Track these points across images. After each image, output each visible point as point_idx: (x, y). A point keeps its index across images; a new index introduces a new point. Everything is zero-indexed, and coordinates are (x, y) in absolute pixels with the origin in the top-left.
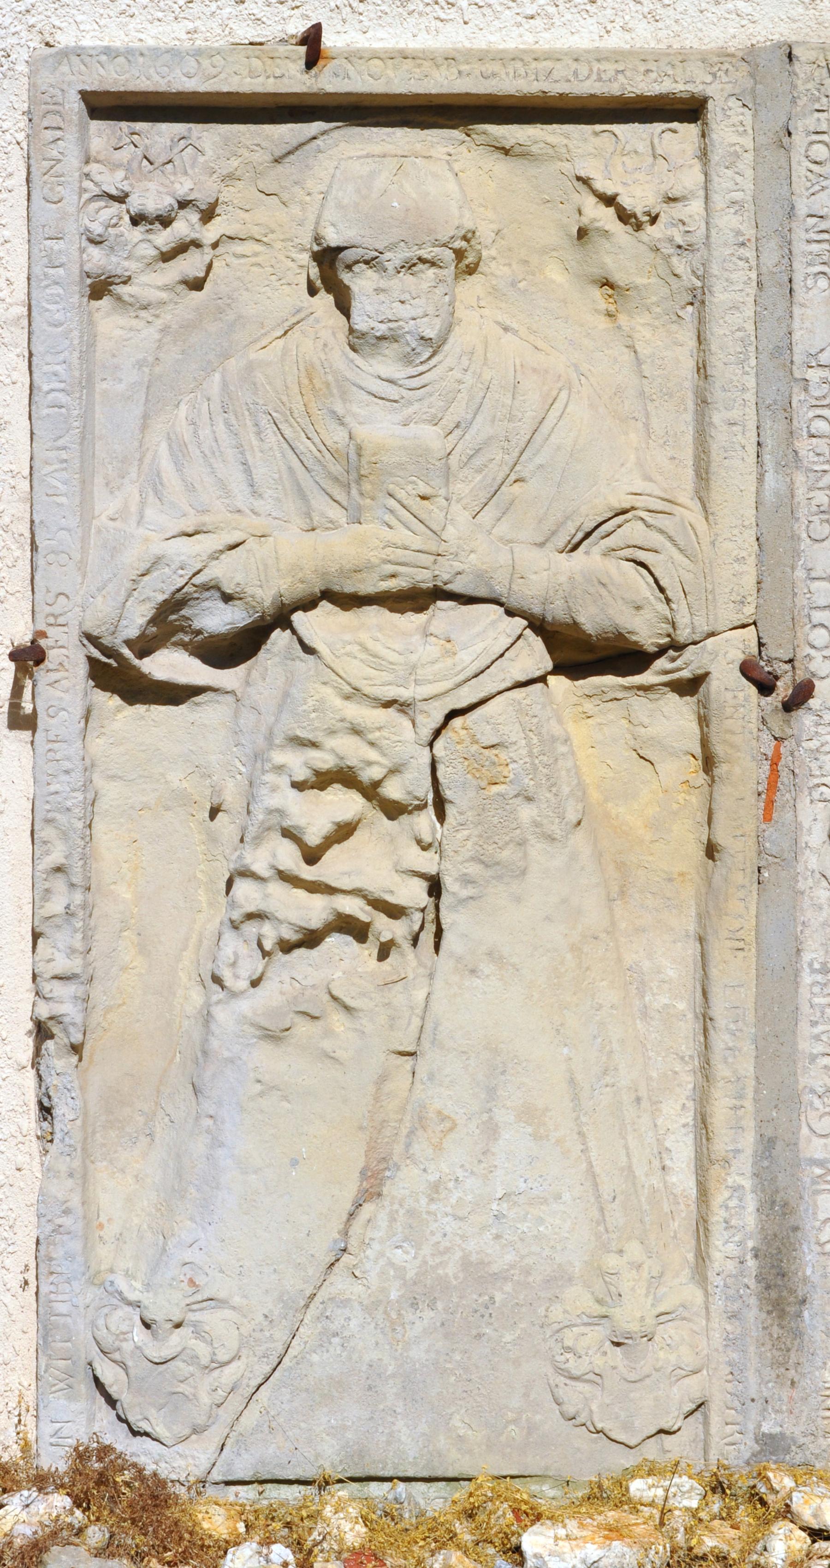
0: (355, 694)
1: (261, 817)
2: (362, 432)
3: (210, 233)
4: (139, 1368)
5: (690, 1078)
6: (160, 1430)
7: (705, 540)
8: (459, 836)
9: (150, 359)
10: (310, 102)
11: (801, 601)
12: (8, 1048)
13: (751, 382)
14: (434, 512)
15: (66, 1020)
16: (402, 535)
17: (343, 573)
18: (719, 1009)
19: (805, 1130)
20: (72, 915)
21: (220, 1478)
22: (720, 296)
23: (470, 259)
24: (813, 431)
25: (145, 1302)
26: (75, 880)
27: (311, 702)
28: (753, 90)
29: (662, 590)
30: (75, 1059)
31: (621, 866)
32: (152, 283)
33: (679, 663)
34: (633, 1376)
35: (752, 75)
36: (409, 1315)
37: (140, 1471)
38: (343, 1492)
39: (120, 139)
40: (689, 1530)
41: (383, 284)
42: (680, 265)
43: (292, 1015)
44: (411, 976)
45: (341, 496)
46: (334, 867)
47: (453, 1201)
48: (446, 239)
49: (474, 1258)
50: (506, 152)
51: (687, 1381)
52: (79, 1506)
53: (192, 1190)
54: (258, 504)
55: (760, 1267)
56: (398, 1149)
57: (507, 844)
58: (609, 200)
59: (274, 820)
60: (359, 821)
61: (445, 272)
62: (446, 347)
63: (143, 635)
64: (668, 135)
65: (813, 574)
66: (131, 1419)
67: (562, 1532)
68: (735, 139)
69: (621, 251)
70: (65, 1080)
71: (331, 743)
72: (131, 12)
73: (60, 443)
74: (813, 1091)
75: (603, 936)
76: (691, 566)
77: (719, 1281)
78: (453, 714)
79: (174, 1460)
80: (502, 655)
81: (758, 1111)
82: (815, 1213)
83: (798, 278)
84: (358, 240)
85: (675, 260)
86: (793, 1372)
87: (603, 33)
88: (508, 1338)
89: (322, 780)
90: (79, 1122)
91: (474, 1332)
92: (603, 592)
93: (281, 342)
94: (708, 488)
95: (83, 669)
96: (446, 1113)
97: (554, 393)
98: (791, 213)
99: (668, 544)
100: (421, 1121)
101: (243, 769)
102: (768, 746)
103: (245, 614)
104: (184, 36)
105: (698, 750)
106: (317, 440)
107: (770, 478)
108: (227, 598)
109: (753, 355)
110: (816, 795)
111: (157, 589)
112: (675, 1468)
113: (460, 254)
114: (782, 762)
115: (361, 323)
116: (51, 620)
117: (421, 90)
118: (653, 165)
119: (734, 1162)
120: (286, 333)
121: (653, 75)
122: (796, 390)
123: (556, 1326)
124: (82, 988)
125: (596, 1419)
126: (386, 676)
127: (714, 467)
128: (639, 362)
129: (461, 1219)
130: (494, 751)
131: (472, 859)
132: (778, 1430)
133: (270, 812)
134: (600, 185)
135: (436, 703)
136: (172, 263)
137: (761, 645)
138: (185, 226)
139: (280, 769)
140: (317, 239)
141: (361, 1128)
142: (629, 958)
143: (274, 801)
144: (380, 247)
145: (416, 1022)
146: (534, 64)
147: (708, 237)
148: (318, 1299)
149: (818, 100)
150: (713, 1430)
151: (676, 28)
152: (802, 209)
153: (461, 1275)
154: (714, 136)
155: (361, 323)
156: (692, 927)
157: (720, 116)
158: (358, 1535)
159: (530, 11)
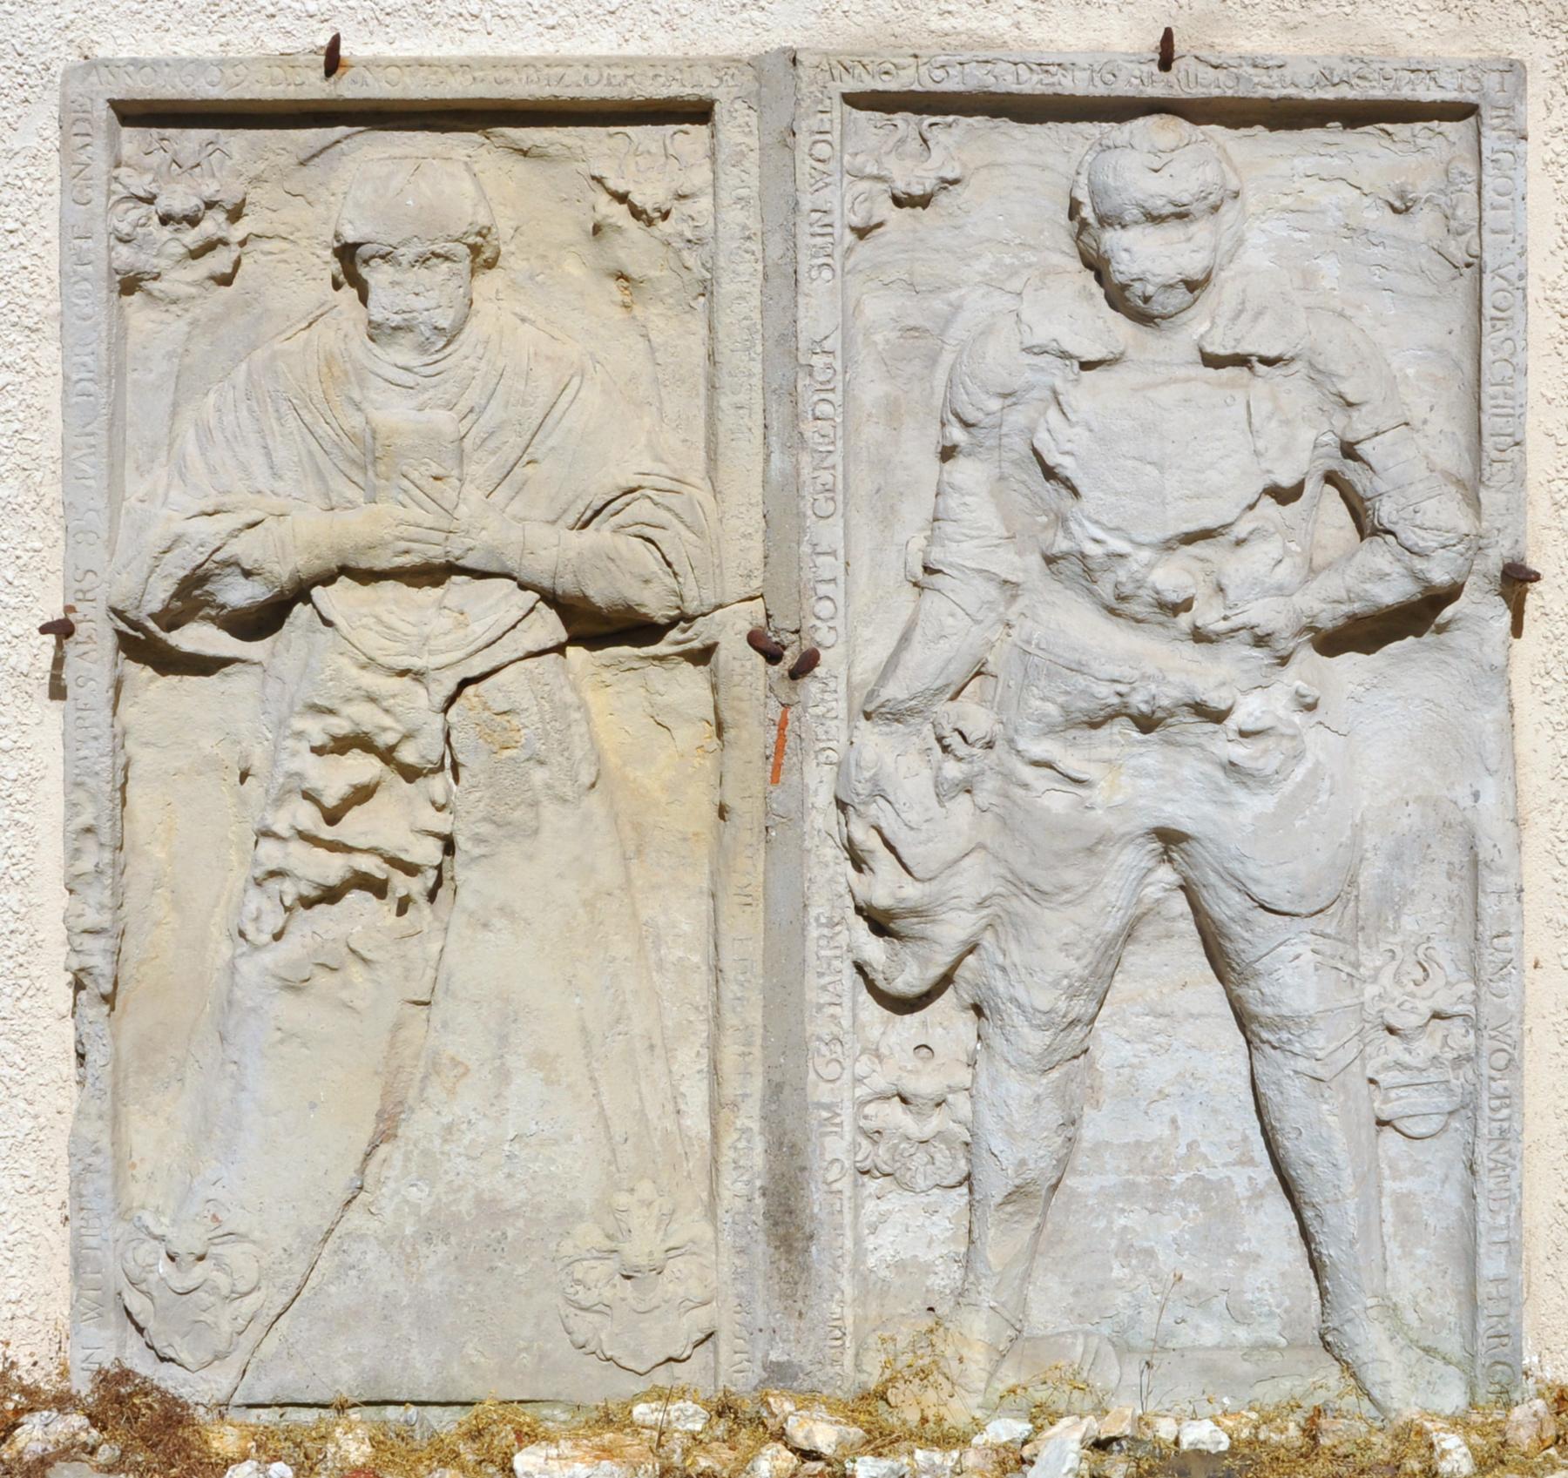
0: (369, 664)
1: (281, 780)
2: (378, 417)
3: (238, 232)
5: (704, 1027)
6: (184, 1356)
8: (471, 797)
9: (180, 350)
10: (334, 108)
11: (807, 574)
12: (49, 999)
13: (757, 368)
14: (447, 491)
15: (96, 971)
16: (415, 514)
17: (358, 549)
19: (812, 1076)
20: (101, 873)
21: (240, 1401)
22: (727, 288)
23: (488, 253)
24: (818, 414)
25: (169, 1236)
26: (103, 840)
27: (328, 672)
28: (758, 93)
29: (669, 565)
30: (106, 1009)
31: (637, 827)
32: (181, 279)
33: (689, 634)
34: (642, 1308)
35: (757, 79)
36: (423, 1249)
37: (164, 1394)
38: (354, 1415)
39: (150, 144)
40: (686, 1452)
41: (398, 277)
42: (690, 259)
43: (311, 967)
44: (426, 930)
45: (358, 478)
46: (352, 828)
47: (466, 1142)
48: (458, 235)
49: (486, 1196)
50: (525, 153)
51: (695, 1312)
52: (94, 1426)
53: (218, 1132)
54: (279, 486)
55: (768, 1205)
56: (413, 1093)
57: (518, 805)
58: (622, 198)
59: (295, 783)
60: (377, 784)
61: (459, 266)
62: (462, 337)
63: (166, 610)
64: (679, 136)
65: (819, 549)
66: (157, 1346)
67: (553, 1452)
68: (740, 139)
69: (636, 247)
70: (97, 1028)
71: (348, 710)
72: (166, 26)
73: (89, 429)
74: (819, 1039)
75: (617, 892)
76: (699, 542)
77: (727, 1218)
78: (465, 683)
79: (195, 1386)
80: (514, 627)
81: (766, 1057)
82: (822, 1154)
84: (372, 236)
85: (685, 253)
86: (800, 1304)
87: (621, 41)
88: (520, 1270)
89: (341, 745)
90: (109, 1068)
91: (487, 1265)
92: (611, 565)
93: (305, 333)
94: (716, 469)
95: (110, 641)
96: (459, 1058)
97: (566, 380)
98: (796, 207)
99: (675, 521)
100: (435, 1067)
101: (270, 736)
102: (775, 712)
103: (264, 589)
104: (217, 49)
105: (712, 717)
106: (335, 425)
107: (776, 458)
108: (247, 574)
109: (759, 342)
110: (822, 758)
111: (178, 566)
112: (683, 1394)
113: (475, 250)
114: (789, 727)
116: (80, 596)
117: (436, 96)
118: (665, 165)
119: (742, 1106)
120: (310, 325)
121: (662, 80)
122: (801, 375)
123: (567, 1260)
124: (112, 942)
125: (605, 1348)
126: (401, 647)
127: (721, 449)
129: (474, 1159)
130: (506, 718)
131: (484, 819)
132: (785, 1358)
133: (290, 775)
134: (612, 184)
135: (448, 672)
136: (201, 260)
137: (768, 616)
138: (212, 225)
139: (299, 735)
140: (337, 236)
141: (376, 1073)
142: (644, 915)
143: (294, 765)
144: (394, 242)
145: (430, 973)
146: (546, 70)
147: (716, 232)
148: (336, 1233)
149: (821, 101)
150: (722, 1359)
151: (693, 36)
153: (474, 1212)
154: (721, 136)
156: (705, 885)
157: (726, 118)
158: (363, 1455)
159: (551, 22)
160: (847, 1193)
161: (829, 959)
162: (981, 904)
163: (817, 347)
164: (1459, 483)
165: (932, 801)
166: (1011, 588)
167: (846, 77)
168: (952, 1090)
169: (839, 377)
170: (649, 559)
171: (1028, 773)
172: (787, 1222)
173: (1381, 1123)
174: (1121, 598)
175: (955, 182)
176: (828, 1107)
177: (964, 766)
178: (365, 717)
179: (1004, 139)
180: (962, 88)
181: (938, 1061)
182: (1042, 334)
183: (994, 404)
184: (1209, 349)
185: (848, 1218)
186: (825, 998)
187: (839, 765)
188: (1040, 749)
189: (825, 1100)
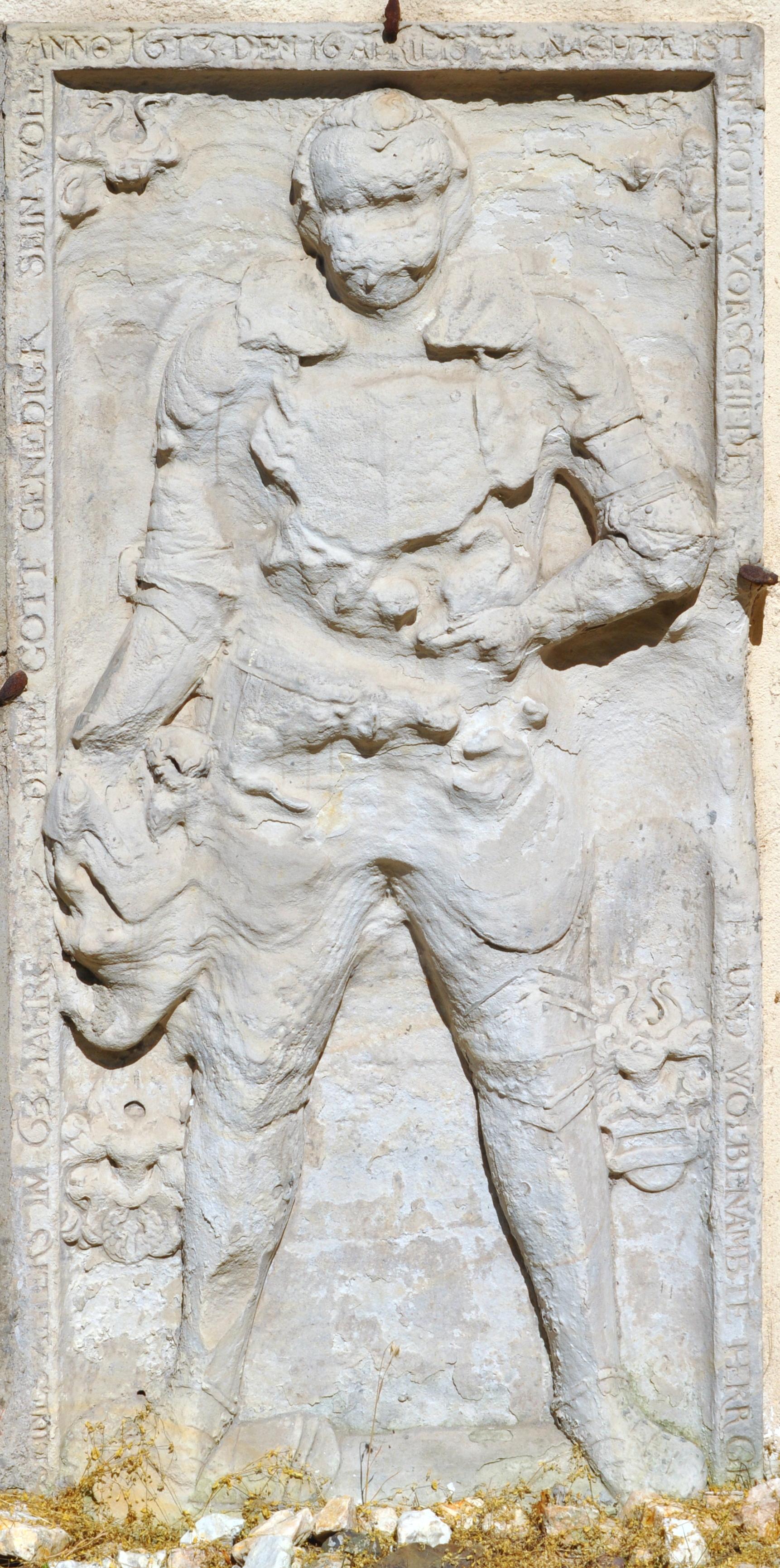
11: (14, 592)
19: (16, 1139)
83: (12, 261)
160: (53, 1267)
161: (35, 1010)
162: (194, 947)
163: (27, 346)
167: (58, 53)
168: (164, 1150)
169: (50, 377)
171: (244, 803)
173: (615, 1176)
175: (172, 164)
176: (32, 1172)
177: (176, 797)
181: (151, 1117)
183: (211, 404)
184: (433, 341)
185: (53, 1294)
186: (31, 1053)
187: (47, 797)
188: (255, 777)
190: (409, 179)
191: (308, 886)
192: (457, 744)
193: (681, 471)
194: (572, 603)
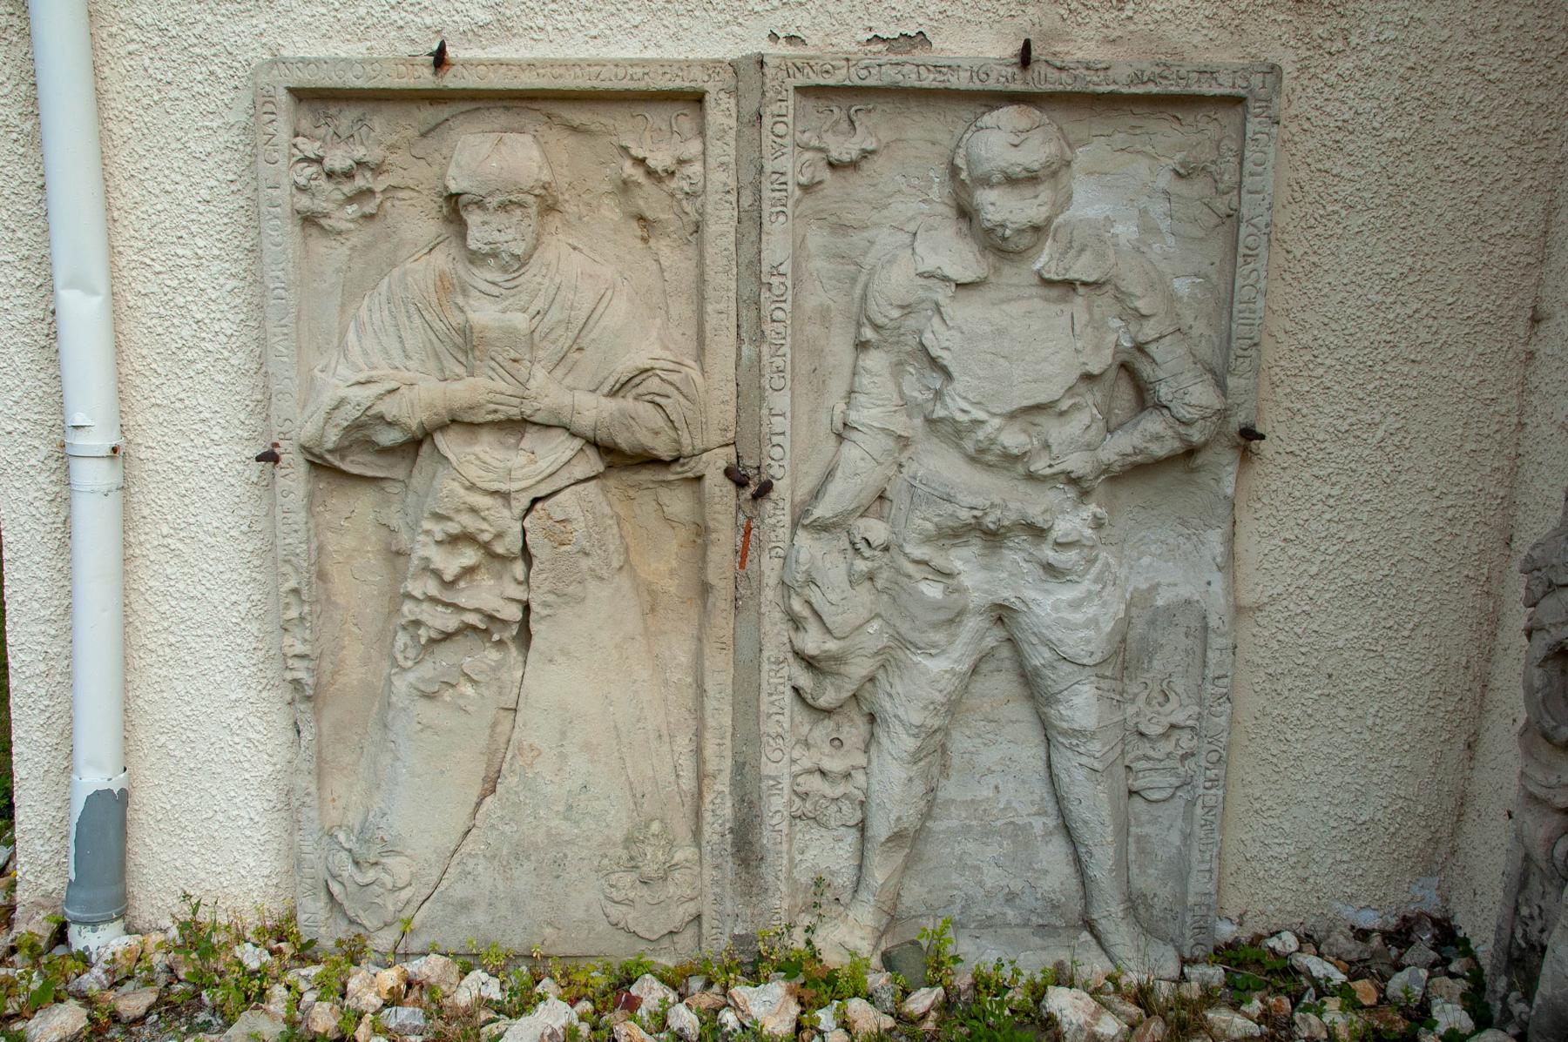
0: (472, 487)
4: (352, 888)
7: (701, 389)
11: (765, 429)
16: (500, 385)
18: (710, 685)
19: (764, 759)
22: (712, 229)
31: (650, 592)
45: (463, 359)
54: (408, 363)
69: (651, 200)
71: (458, 518)
78: (535, 501)
83: (765, 215)
84: (468, 189)
89: (454, 540)
98: (761, 171)
115: (473, 244)
117: (512, 87)
126: (491, 476)
128: (662, 270)
139: (428, 532)
145: (516, 691)
152: (768, 168)
155: (473, 244)
160: (786, 831)
161: (777, 685)
162: (877, 654)
163: (775, 270)
164: (1212, 371)
165: (846, 586)
166: (903, 442)
167: (798, 75)
168: (854, 767)
169: (790, 292)
170: (658, 420)
171: (910, 568)
172: (745, 846)
173: (1131, 793)
174: (982, 451)
175: (873, 152)
176: (774, 778)
177: (869, 564)
178: (470, 523)
179: (909, 121)
180: (880, 83)
181: (846, 748)
182: (929, 265)
183: (896, 313)
184: (1047, 276)
185: (785, 847)
186: (774, 710)
187: (785, 558)
188: (918, 552)
189: (773, 774)
190: (1036, 166)
191: (951, 621)
192: (1050, 539)
193: (1204, 363)
194: (1130, 450)
